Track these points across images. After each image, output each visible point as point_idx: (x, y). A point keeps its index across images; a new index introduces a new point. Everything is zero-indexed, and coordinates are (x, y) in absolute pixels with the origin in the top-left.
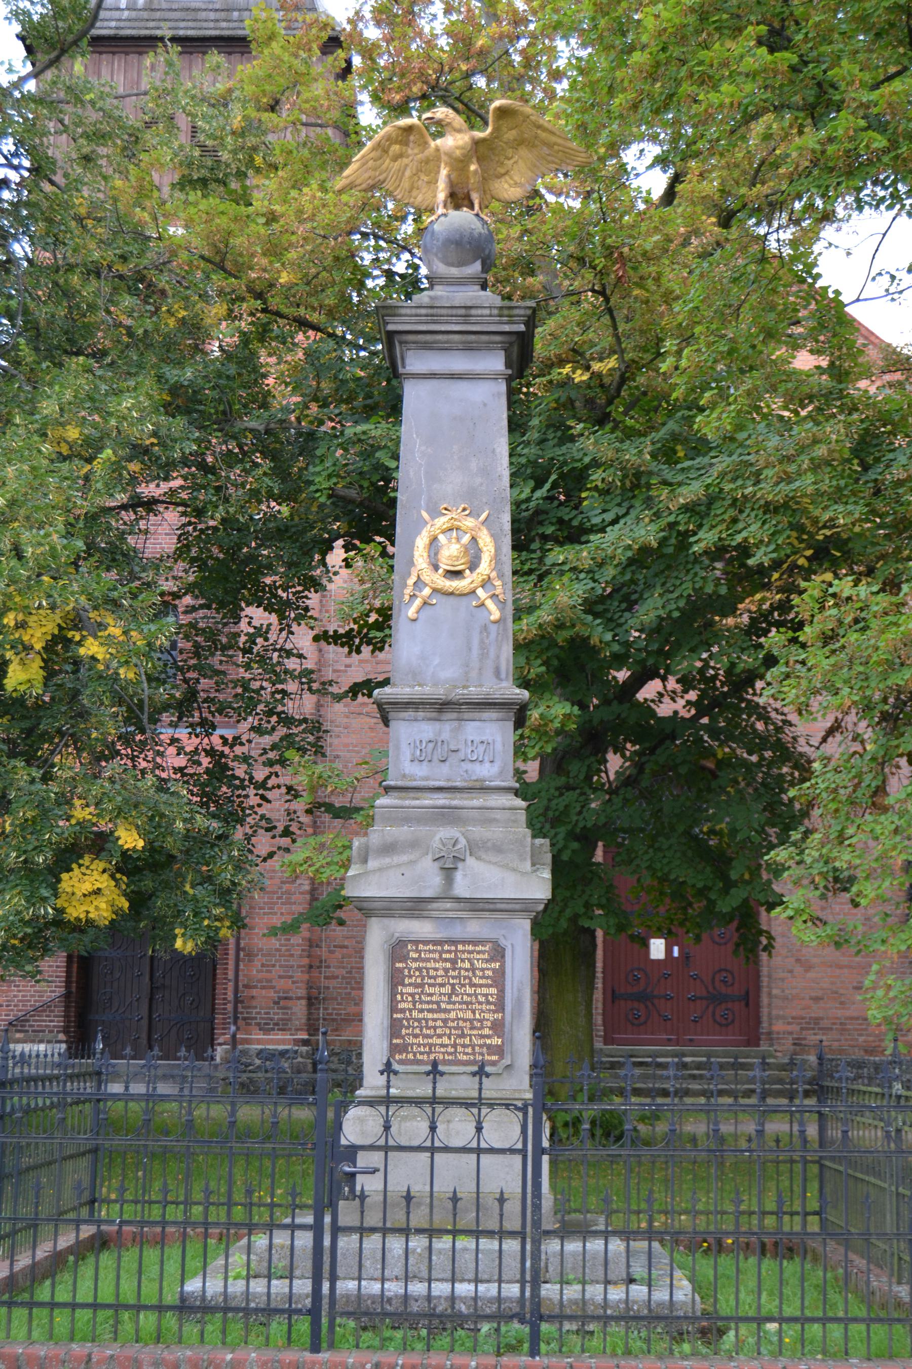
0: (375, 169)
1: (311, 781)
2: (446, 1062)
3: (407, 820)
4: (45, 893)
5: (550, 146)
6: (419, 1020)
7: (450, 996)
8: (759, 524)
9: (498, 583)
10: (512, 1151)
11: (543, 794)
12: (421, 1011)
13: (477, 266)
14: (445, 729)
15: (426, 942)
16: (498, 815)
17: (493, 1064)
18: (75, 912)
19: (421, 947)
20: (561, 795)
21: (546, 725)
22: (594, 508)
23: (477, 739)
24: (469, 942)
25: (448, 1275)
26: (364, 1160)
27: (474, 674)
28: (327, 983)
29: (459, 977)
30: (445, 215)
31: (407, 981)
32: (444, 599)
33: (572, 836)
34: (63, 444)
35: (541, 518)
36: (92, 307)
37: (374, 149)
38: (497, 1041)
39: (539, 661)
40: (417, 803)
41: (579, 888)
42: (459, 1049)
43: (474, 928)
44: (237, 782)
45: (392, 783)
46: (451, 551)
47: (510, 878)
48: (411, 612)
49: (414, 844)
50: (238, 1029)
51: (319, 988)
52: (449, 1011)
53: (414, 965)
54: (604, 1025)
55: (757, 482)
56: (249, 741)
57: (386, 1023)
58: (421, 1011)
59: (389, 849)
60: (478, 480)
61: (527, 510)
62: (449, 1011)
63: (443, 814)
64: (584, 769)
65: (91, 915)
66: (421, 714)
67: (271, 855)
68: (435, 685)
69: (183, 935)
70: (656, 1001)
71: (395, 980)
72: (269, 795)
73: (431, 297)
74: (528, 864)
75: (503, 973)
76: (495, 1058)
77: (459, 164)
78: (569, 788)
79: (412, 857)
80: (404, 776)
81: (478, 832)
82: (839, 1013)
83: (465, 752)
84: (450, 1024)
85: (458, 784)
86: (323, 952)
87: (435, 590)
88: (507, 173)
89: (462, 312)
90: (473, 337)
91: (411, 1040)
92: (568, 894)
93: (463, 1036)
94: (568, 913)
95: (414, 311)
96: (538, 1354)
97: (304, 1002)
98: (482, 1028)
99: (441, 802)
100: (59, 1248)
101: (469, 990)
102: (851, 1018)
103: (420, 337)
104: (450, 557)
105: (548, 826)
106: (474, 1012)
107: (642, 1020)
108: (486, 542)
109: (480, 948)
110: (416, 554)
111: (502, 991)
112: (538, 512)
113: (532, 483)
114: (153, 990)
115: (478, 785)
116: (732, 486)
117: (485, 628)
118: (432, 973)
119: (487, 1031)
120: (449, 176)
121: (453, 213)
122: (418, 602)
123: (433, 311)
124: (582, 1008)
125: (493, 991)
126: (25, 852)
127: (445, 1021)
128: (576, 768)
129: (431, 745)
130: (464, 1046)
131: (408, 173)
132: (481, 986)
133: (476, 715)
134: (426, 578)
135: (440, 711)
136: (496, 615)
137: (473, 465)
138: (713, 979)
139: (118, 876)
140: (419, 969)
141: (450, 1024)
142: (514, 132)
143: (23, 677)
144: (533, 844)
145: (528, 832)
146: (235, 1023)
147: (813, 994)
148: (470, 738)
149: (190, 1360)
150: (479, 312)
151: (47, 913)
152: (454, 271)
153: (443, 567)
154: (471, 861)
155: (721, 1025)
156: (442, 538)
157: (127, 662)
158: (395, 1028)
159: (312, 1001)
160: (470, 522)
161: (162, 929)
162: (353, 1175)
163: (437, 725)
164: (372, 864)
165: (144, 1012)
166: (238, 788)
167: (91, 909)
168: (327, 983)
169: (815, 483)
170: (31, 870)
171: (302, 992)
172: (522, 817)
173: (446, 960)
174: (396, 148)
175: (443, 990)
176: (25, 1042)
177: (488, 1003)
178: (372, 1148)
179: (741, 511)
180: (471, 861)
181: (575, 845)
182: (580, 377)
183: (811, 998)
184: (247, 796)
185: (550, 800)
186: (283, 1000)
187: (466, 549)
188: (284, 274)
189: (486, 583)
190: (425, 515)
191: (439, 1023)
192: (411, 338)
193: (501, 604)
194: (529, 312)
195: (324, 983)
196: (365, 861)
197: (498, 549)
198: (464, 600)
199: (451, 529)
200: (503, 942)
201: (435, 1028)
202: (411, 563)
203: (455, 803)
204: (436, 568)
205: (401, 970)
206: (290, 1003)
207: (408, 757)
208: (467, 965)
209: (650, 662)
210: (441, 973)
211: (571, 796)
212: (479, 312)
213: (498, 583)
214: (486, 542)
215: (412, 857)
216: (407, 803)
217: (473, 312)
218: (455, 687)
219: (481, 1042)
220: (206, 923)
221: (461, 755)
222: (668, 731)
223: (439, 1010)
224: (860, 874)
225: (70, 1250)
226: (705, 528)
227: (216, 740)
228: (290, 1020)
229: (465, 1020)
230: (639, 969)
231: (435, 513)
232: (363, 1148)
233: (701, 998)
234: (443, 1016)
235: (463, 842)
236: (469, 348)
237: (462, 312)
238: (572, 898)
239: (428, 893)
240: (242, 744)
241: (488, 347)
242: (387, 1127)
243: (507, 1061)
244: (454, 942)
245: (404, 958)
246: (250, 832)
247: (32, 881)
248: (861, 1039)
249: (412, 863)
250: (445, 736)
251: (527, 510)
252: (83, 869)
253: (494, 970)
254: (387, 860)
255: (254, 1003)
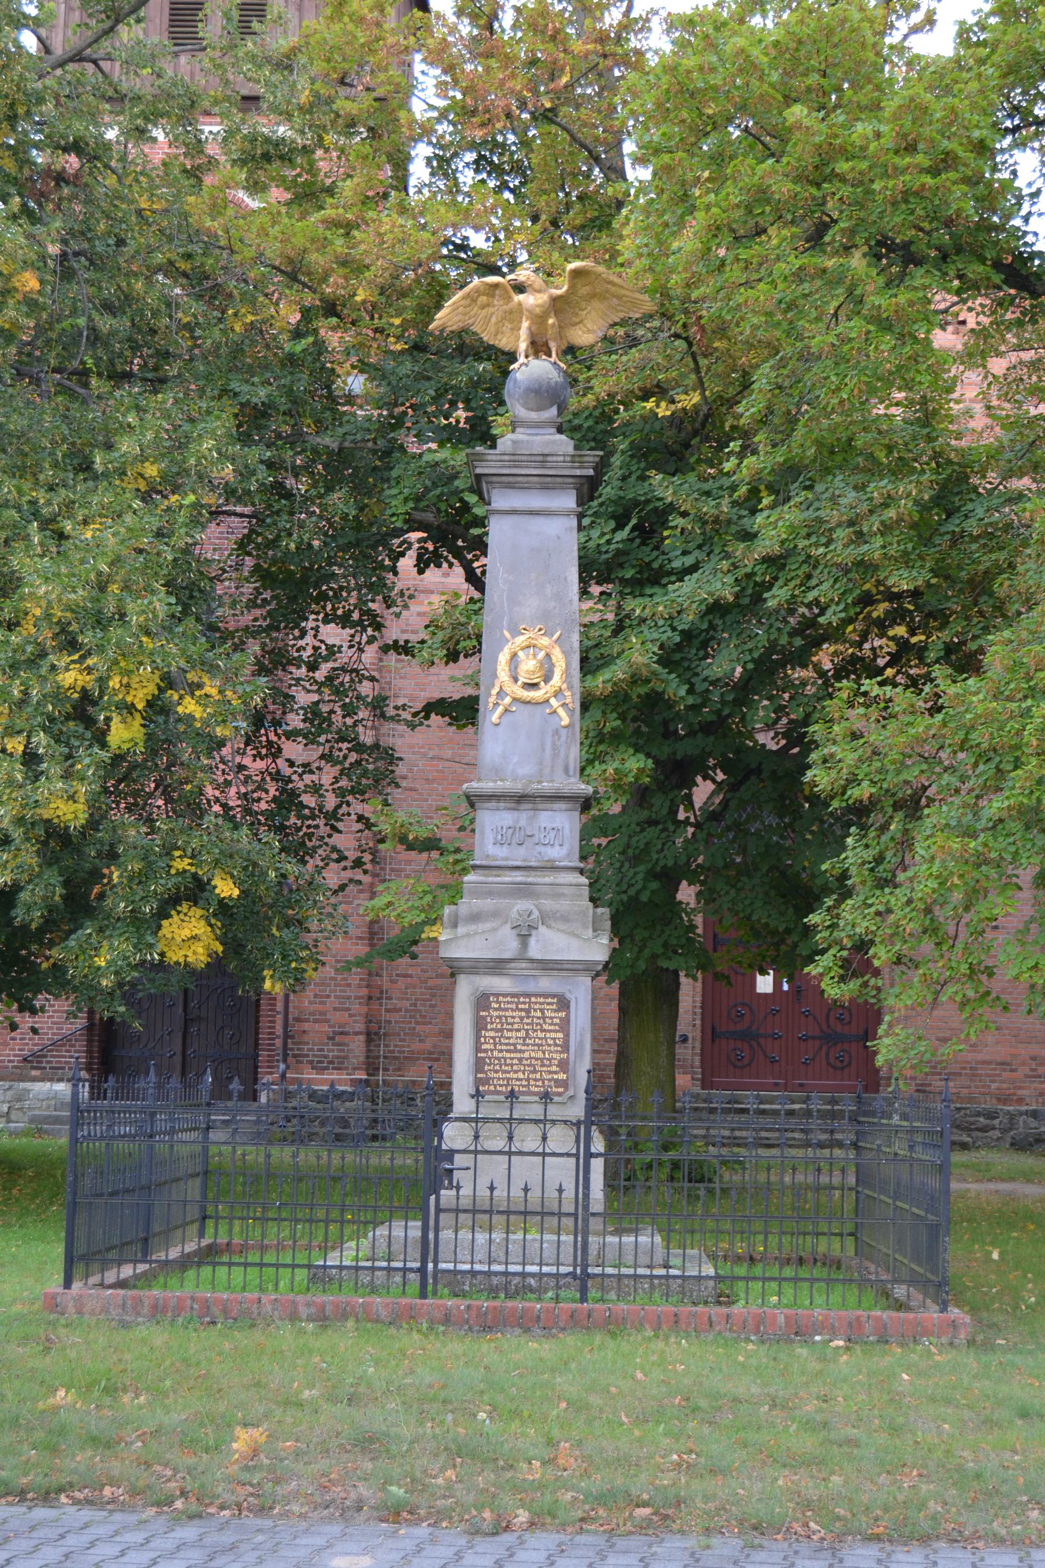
0: (465, 314)
1: (394, 828)
2: (524, 1093)
3: (490, 894)
4: (150, 939)
5: (619, 298)
6: (499, 1059)
7: (524, 1039)
8: (831, 581)
9: (568, 693)
10: (568, 1155)
11: (624, 830)
12: (501, 1051)
13: (554, 411)
14: (522, 817)
15: (505, 995)
16: (566, 890)
17: (559, 1094)
18: (175, 956)
19: (501, 999)
20: (643, 830)
21: (620, 779)
22: (675, 548)
23: (549, 826)
24: (541, 996)
25: (521, 1259)
26: (459, 1160)
27: (547, 771)
28: (389, 1016)
29: (532, 1024)
30: (527, 365)
31: (489, 1027)
32: (522, 707)
33: (652, 875)
34: (140, 480)
35: (622, 559)
36: (155, 313)
37: (463, 298)
38: (562, 1076)
39: (615, 715)
40: (499, 879)
41: (659, 927)
42: (532, 1082)
43: (546, 983)
44: (307, 811)
45: (478, 862)
46: (528, 665)
47: (575, 943)
48: (495, 718)
49: (495, 914)
50: (288, 1067)
51: (379, 1022)
52: (523, 1052)
53: (495, 1014)
54: (702, 1066)
55: (830, 542)
56: (319, 769)
57: (472, 1060)
58: (501, 1051)
59: (475, 918)
60: (552, 604)
61: (606, 552)
62: (523, 1052)
63: (520, 890)
64: (668, 804)
65: (189, 959)
66: (502, 805)
67: (342, 888)
68: (514, 780)
69: (272, 977)
70: (762, 1041)
71: (479, 1026)
72: (340, 825)
73: (514, 442)
74: (590, 931)
75: (569, 1021)
76: (561, 1090)
77: (539, 319)
78: (652, 823)
79: (494, 925)
80: (488, 856)
81: (548, 904)
82: (970, 1056)
83: (539, 836)
84: (525, 1062)
85: (533, 864)
86: (384, 982)
87: (515, 699)
88: (581, 322)
89: (540, 458)
90: (549, 479)
91: (492, 1075)
92: (646, 934)
93: (535, 1072)
94: (647, 952)
95: (499, 458)
96: (586, 1301)
97: (362, 1038)
98: (550, 1065)
99: (519, 879)
100: (186, 1251)
101: (540, 1035)
102: (984, 1062)
103: (503, 479)
104: (528, 672)
105: (627, 865)
106: (544, 1052)
107: (746, 1061)
108: (558, 656)
109: (550, 1000)
110: (499, 668)
111: (567, 1036)
112: (619, 553)
113: (612, 524)
114: (187, 1022)
115: (549, 864)
116: (807, 542)
117: (556, 732)
118: (510, 1020)
119: (554, 1068)
120: (529, 328)
121: (534, 362)
122: (500, 709)
123: (515, 458)
124: (664, 1049)
125: (560, 1035)
126: (133, 902)
127: (520, 1059)
128: (659, 804)
129: (510, 831)
130: (535, 1080)
131: (494, 320)
132: (550, 1031)
133: (549, 806)
134: (507, 689)
135: (518, 802)
136: (566, 720)
137: (548, 590)
138: (828, 1016)
139: (213, 921)
140: (499, 1017)
141: (525, 1062)
142: (587, 288)
143: (126, 735)
144: (594, 914)
145: (591, 904)
146: (285, 1061)
147: (941, 1035)
148: (543, 825)
149: (333, 1302)
150: (555, 459)
151: (153, 959)
152: (534, 416)
153: (522, 680)
154: (542, 929)
155: (834, 1067)
156: (521, 654)
157: (224, 721)
158: (479, 1065)
159: (371, 1037)
160: (545, 641)
161: (251, 971)
162: (451, 1171)
163: (516, 814)
164: (461, 930)
165: (178, 1047)
166: (308, 818)
167: (189, 954)
168: (389, 1016)
169: (884, 547)
170: (136, 918)
171: (360, 1027)
172: (586, 892)
173: (521, 1010)
174: (483, 299)
175: (519, 1035)
176: (42, 1080)
177: (556, 1045)
178: (465, 1151)
179: (815, 567)
180: (542, 929)
181: (654, 885)
182: (664, 411)
183: (938, 1039)
184: (317, 827)
185: (630, 837)
186: (338, 1035)
187: (541, 663)
188: (360, 291)
189: (558, 693)
190: (507, 634)
191: (515, 1061)
192: (495, 479)
193: (571, 712)
194: (597, 459)
195: (384, 1016)
196: (455, 925)
197: (568, 665)
198: (539, 708)
199: (528, 647)
200: (568, 996)
201: (512, 1065)
202: (495, 676)
203: (530, 880)
204: (516, 680)
205: (484, 1018)
206: (346, 1039)
207: (492, 841)
208: (539, 1014)
209: (726, 712)
210: (517, 1020)
211: (652, 832)
212: (555, 459)
213: (568, 693)
214: (558, 656)
215: (494, 925)
216: (490, 879)
217: (549, 459)
218: (531, 782)
219: (550, 1077)
220: (293, 965)
221: (536, 839)
222: (754, 765)
223: (516, 1051)
224: (878, 939)
225: (195, 1253)
226: (780, 582)
227: (281, 763)
228: (346, 1057)
229: (537, 1059)
230: (743, 1005)
231: (515, 632)
232: (458, 1152)
233: (814, 1038)
234: (518, 1055)
235: (536, 914)
236: (545, 487)
237: (540, 458)
238: (651, 938)
239: (507, 955)
240: (311, 772)
241: (562, 487)
242: (476, 1137)
243: (571, 1093)
244: (528, 995)
245: (487, 1008)
246: (321, 864)
247: (138, 929)
248: (994, 1086)
249: (494, 930)
250: (523, 823)
251: (606, 552)
252: (182, 916)
253: (561, 1019)
254: (474, 927)
255: (306, 1038)
